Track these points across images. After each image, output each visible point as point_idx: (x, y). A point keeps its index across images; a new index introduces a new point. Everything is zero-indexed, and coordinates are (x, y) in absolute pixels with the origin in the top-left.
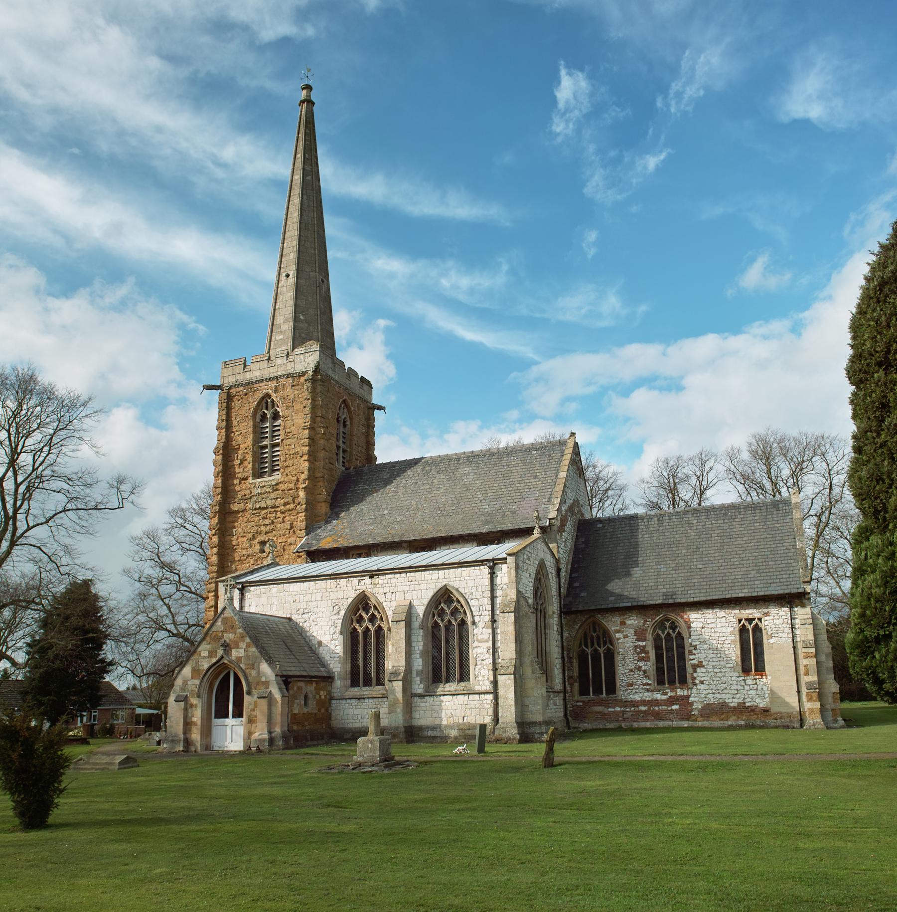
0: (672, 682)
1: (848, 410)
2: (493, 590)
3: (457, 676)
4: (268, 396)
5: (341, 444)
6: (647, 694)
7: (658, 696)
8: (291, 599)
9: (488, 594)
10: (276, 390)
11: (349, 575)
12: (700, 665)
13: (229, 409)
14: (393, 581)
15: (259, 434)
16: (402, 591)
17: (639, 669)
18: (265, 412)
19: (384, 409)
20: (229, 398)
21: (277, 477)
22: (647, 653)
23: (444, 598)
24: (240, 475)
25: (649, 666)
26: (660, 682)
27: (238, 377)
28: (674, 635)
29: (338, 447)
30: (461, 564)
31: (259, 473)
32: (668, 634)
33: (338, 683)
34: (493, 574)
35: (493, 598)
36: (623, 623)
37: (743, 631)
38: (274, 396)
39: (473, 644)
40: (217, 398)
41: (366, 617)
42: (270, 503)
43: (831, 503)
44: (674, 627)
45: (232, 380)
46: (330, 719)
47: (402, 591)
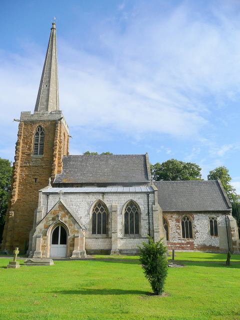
0: (187, 237)
2: (148, 203)
6: (180, 241)
7: (183, 242)
9: (147, 204)
12: (197, 232)
17: (177, 232)
22: (180, 227)
25: (181, 231)
26: (184, 237)
28: (188, 222)
32: (99, 213)
34: (148, 197)
35: (148, 205)
36: (172, 217)
37: (211, 222)
41: (99, 209)
44: (188, 219)
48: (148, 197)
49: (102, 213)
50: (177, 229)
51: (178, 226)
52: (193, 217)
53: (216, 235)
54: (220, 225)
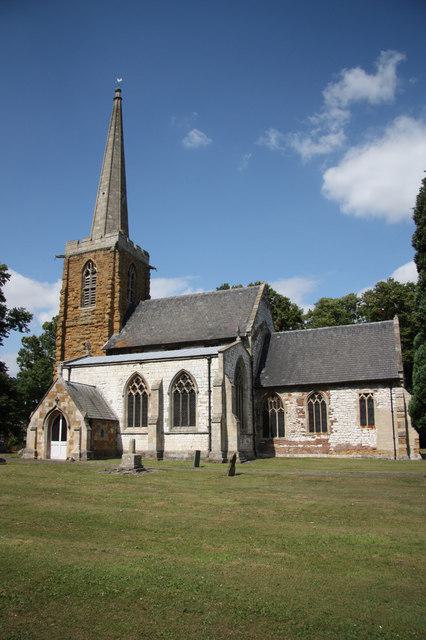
0: (318, 431)
7: (310, 439)
12: (335, 421)
21: (94, 307)
23: (183, 375)
25: (305, 421)
26: (311, 430)
30: (192, 357)
33: (121, 425)
34: (209, 363)
35: (209, 377)
37: (362, 401)
47: (159, 373)
48: (209, 363)
49: (141, 394)
50: (301, 417)
51: (302, 411)
52: (328, 395)
53: (372, 425)
54: (379, 407)
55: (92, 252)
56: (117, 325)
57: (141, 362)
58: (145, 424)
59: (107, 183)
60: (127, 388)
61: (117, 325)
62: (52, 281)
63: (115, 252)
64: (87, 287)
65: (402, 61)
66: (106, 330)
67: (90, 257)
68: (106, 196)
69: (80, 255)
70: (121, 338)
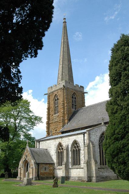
1: (43, 42)
3: (78, 163)
4: (56, 94)
5: (74, 104)
8: (47, 144)
9: (83, 142)
10: (57, 93)
11: (55, 138)
13: (49, 99)
14: (65, 139)
15: (55, 103)
16: (67, 142)
18: (56, 99)
19: (87, 93)
20: (49, 96)
21: (58, 114)
23: (75, 143)
24: (52, 114)
27: (51, 91)
29: (73, 105)
30: (78, 134)
31: (55, 114)
33: (56, 165)
34: (84, 136)
35: (84, 142)
38: (57, 94)
39: (81, 157)
40: (47, 97)
42: (57, 120)
43: (18, 115)
45: (49, 92)
46: (54, 174)
47: (67, 142)
48: (84, 136)
49: (60, 151)
55: (56, 91)
56: (66, 121)
57: (61, 137)
58: (61, 165)
59: (62, 59)
60: (57, 149)
61: (66, 121)
62: (104, 73)
63: (64, 89)
64: (56, 106)
65: (32, 93)
66: (62, 124)
67: (55, 93)
68: (62, 65)
69: (53, 92)
70: (68, 127)
